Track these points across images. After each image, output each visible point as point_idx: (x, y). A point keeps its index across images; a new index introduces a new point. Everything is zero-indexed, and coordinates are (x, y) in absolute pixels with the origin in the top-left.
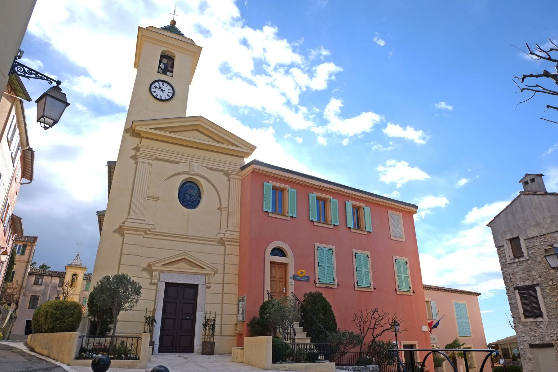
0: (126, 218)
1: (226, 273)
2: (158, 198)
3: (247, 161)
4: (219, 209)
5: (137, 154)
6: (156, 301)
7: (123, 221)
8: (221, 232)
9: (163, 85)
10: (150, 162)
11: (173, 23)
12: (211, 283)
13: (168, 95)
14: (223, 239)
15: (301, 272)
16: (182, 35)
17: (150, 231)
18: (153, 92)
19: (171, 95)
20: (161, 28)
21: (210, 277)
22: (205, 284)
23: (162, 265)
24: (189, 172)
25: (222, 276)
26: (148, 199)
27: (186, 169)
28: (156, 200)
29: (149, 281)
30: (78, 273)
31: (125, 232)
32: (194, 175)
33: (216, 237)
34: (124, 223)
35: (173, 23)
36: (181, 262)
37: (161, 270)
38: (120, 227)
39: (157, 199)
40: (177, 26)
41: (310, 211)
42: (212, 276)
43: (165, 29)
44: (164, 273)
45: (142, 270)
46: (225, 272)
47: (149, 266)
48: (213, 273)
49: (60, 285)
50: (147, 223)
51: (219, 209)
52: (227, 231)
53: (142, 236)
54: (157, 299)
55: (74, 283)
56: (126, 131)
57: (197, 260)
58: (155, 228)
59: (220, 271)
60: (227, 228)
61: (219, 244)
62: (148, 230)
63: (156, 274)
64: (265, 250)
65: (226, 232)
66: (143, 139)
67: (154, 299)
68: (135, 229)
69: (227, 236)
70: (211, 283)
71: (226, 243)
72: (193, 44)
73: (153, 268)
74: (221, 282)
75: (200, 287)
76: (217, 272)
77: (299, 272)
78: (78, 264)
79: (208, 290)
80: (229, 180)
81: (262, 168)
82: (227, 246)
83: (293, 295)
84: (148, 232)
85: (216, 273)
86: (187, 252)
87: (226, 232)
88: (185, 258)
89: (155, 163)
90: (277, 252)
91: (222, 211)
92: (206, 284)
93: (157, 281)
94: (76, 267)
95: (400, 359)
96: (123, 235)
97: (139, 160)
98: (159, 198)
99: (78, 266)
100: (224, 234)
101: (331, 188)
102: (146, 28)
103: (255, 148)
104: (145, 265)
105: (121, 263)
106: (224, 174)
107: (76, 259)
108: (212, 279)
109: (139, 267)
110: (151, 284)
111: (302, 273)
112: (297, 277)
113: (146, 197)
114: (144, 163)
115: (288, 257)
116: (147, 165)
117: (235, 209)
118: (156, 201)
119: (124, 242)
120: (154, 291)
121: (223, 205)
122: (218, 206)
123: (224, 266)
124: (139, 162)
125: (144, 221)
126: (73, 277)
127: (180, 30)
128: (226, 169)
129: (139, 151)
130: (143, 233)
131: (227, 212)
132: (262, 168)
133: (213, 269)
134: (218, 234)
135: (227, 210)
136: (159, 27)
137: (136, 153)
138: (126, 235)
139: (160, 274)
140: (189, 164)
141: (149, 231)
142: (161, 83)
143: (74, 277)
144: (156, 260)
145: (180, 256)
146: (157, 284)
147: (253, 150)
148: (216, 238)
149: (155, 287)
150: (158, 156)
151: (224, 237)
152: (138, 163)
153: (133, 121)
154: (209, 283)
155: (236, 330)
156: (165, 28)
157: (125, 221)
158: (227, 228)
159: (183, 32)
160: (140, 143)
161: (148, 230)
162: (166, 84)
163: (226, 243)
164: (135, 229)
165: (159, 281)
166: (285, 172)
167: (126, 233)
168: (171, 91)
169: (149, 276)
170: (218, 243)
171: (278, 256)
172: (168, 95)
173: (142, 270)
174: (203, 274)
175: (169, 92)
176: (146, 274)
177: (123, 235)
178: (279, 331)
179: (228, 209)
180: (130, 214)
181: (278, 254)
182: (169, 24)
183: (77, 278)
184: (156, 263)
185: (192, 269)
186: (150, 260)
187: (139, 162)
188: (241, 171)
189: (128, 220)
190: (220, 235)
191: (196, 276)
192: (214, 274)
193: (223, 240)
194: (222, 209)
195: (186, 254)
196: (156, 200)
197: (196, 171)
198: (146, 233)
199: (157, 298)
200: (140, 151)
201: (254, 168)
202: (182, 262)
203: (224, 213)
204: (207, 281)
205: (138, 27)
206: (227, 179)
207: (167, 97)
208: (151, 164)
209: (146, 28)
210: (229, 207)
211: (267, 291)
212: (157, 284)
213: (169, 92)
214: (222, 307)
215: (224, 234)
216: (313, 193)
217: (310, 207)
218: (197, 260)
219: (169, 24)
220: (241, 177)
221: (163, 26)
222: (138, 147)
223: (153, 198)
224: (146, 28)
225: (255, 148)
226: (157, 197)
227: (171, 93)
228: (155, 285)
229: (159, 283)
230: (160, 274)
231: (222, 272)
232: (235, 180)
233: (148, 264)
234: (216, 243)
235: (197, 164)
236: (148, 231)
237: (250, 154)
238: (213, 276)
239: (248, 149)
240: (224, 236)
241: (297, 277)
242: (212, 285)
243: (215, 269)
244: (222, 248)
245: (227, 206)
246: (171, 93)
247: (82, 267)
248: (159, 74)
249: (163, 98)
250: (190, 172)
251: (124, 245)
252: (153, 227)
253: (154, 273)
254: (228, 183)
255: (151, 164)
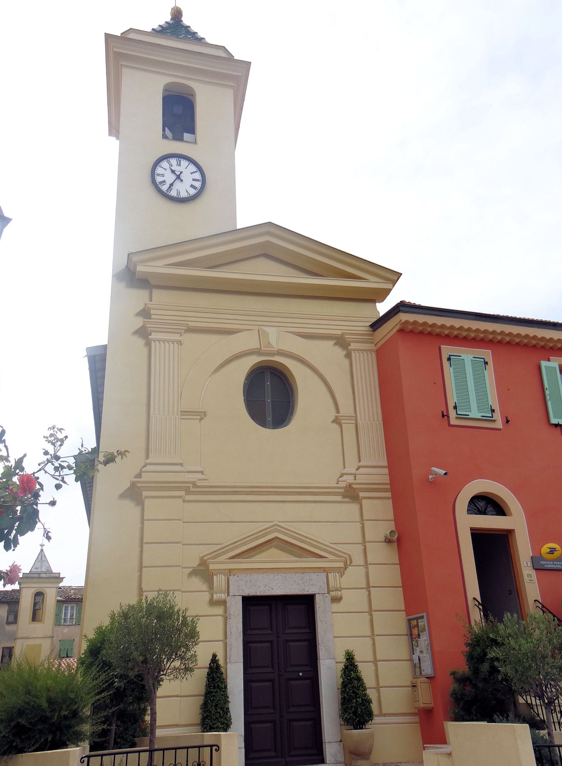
0: (143, 464)
1: (371, 564)
2: (203, 414)
3: (383, 308)
4: (337, 421)
5: (147, 325)
6: (228, 641)
7: (137, 471)
8: (346, 471)
9: (180, 165)
10: (176, 337)
11: (177, 14)
12: (340, 589)
13: (192, 186)
14: (354, 486)
15: (549, 550)
16: (201, 41)
17: (196, 485)
18: (161, 183)
19: (198, 185)
20: (153, 29)
21: (337, 575)
22: (328, 593)
23: (231, 558)
24: (261, 348)
25: (362, 570)
26: (183, 417)
27: (255, 345)
28: (199, 417)
29: (206, 596)
30: (46, 589)
31: (145, 494)
32: (273, 355)
33: (338, 483)
34: (139, 476)
35: (177, 14)
36: (268, 549)
37: (230, 570)
38: (133, 484)
39: (202, 415)
40: (186, 20)
41: (549, 403)
42: (342, 571)
43: (162, 31)
44: (236, 576)
45: (190, 575)
46: (369, 561)
47: (203, 563)
48: (342, 565)
49: (11, 618)
50: (189, 470)
51: (337, 421)
52: (361, 469)
53: (180, 500)
54: (228, 636)
55: (39, 613)
56: (118, 277)
57: (304, 538)
58: (206, 477)
59: (358, 559)
60: (360, 461)
61: (347, 500)
62: (191, 485)
63: (219, 581)
64: (458, 495)
65: (357, 469)
66: (154, 291)
67: (221, 637)
68: (164, 485)
69: (360, 479)
70: (340, 589)
71: (361, 494)
72: (230, 58)
73: (212, 567)
74: (364, 585)
75: (318, 599)
76: (351, 562)
77: (545, 549)
78: (43, 570)
79: (336, 607)
80: (348, 356)
81: (421, 318)
82: (364, 502)
83: (540, 606)
84: (192, 489)
85: (350, 565)
86: (281, 524)
87: (357, 469)
88: (277, 538)
89: (187, 338)
90: (481, 504)
91: (344, 425)
92: (331, 593)
93: (223, 596)
94: (40, 578)
95: (254, 555)
96: (140, 502)
97: (153, 336)
98: (205, 413)
99: (43, 575)
100: (355, 475)
101: (531, 335)
102: (121, 34)
103: (399, 275)
104: (195, 563)
105: (144, 565)
106: (336, 344)
107: (38, 560)
108: (342, 579)
109: (183, 568)
110: (213, 603)
111: (552, 551)
112: (541, 562)
113: (178, 415)
114: (164, 341)
115: (510, 515)
116: (172, 345)
117: (372, 419)
118: (201, 419)
119: (146, 517)
120: (220, 620)
121: (343, 412)
122: (333, 414)
123: (365, 546)
124: (154, 341)
125: (180, 467)
126: (35, 599)
127: (194, 29)
128: (339, 332)
129: (150, 318)
130: (182, 493)
131: (354, 425)
132: (421, 318)
133: (341, 557)
134: (341, 477)
135: (354, 422)
136: (149, 30)
137: (144, 321)
138: (147, 502)
139: (228, 579)
140: (259, 331)
141: (193, 488)
142: (174, 161)
143: (39, 599)
144: (216, 549)
145: (266, 534)
146: (223, 603)
147: (394, 283)
148: (337, 485)
149: (219, 610)
150: (191, 324)
151: (355, 481)
152: (153, 343)
153: (129, 255)
154: (337, 590)
155: (415, 699)
156: (160, 29)
157: (141, 472)
158: (360, 461)
159: (201, 34)
160: (151, 300)
161: (191, 485)
162: (184, 163)
163: (361, 494)
164: (164, 485)
165: (228, 595)
166: (475, 320)
167: (146, 497)
168: (198, 176)
169: (205, 587)
170: (344, 497)
171: (485, 513)
172: (192, 186)
173: (190, 575)
174: (322, 570)
175: (194, 180)
176: (197, 583)
177: (140, 502)
178: (527, 702)
179: (354, 418)
180: (150, 455)
181: (485, 509)
182: (168, 18)
183: (43, 598)
184: (216, 555)
185: (296, 562)
186: (204, 551)
187: (154, 341)
188: (372, 333)
189: (149, 468)
190: (345, 478)
191: (307, 576)
192: (346, 568)
193: (354, 489)
194: (342, 421)
195: (279, 528)
196: (199, 417)
197: (275, 346)
198: (188, 492)
199: (228, 633)
200: (153, 317)
201: (403, 321)
202: (271, 547)
203: (349, 429)
204: (332, 584)
205: (104, 34)
206: (344, 353)
207: (192, 192)
208: (180, 343)
209: (120, 35)
210: (356, 414)
211: (474, 598)
212: (223, 603)
213: (194, 180)
214: (374, 644)
215: (355, 475)
216: (549, 360)
217: (547, 392)
218: (304, 538)
219: (168, 18)
220: (373, 345)
221: (156, 27)
222: (147, 308)
223: (191, 414)
224: (120, 35)
225: (399, 275)
226: (202, 410)
227: (198, 180)
228: (220, 605)
229: (228, 599)
230: (228, 579)
231: (362, 562)
232: (361, 354)
233: (200, 560)
234: (339, 498)
235: (276, 329)
236: (191, 487)
237: (388, 291)
238: (344, 573)
239: (384, 281)
240: (355, 479)
241: (541, 562)
242: (345, 593)
243: (347, 556)
244: (354, 507)
245: (351, 412)
246: (198, 180)
247: (53, 575)
248: (166, 141)
249: (184, 195)
250: (263, 349)
251: (145, 522)
252: (200, 476)
253: (215, 577)
254: (346, 362)
255: (180, 343)
